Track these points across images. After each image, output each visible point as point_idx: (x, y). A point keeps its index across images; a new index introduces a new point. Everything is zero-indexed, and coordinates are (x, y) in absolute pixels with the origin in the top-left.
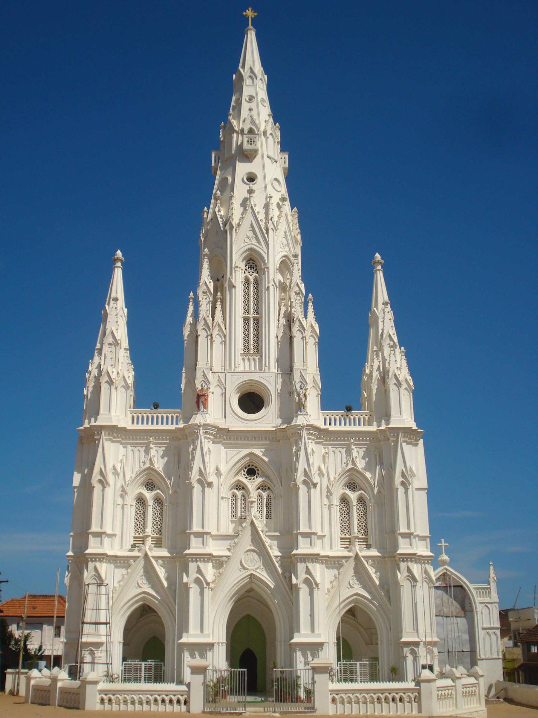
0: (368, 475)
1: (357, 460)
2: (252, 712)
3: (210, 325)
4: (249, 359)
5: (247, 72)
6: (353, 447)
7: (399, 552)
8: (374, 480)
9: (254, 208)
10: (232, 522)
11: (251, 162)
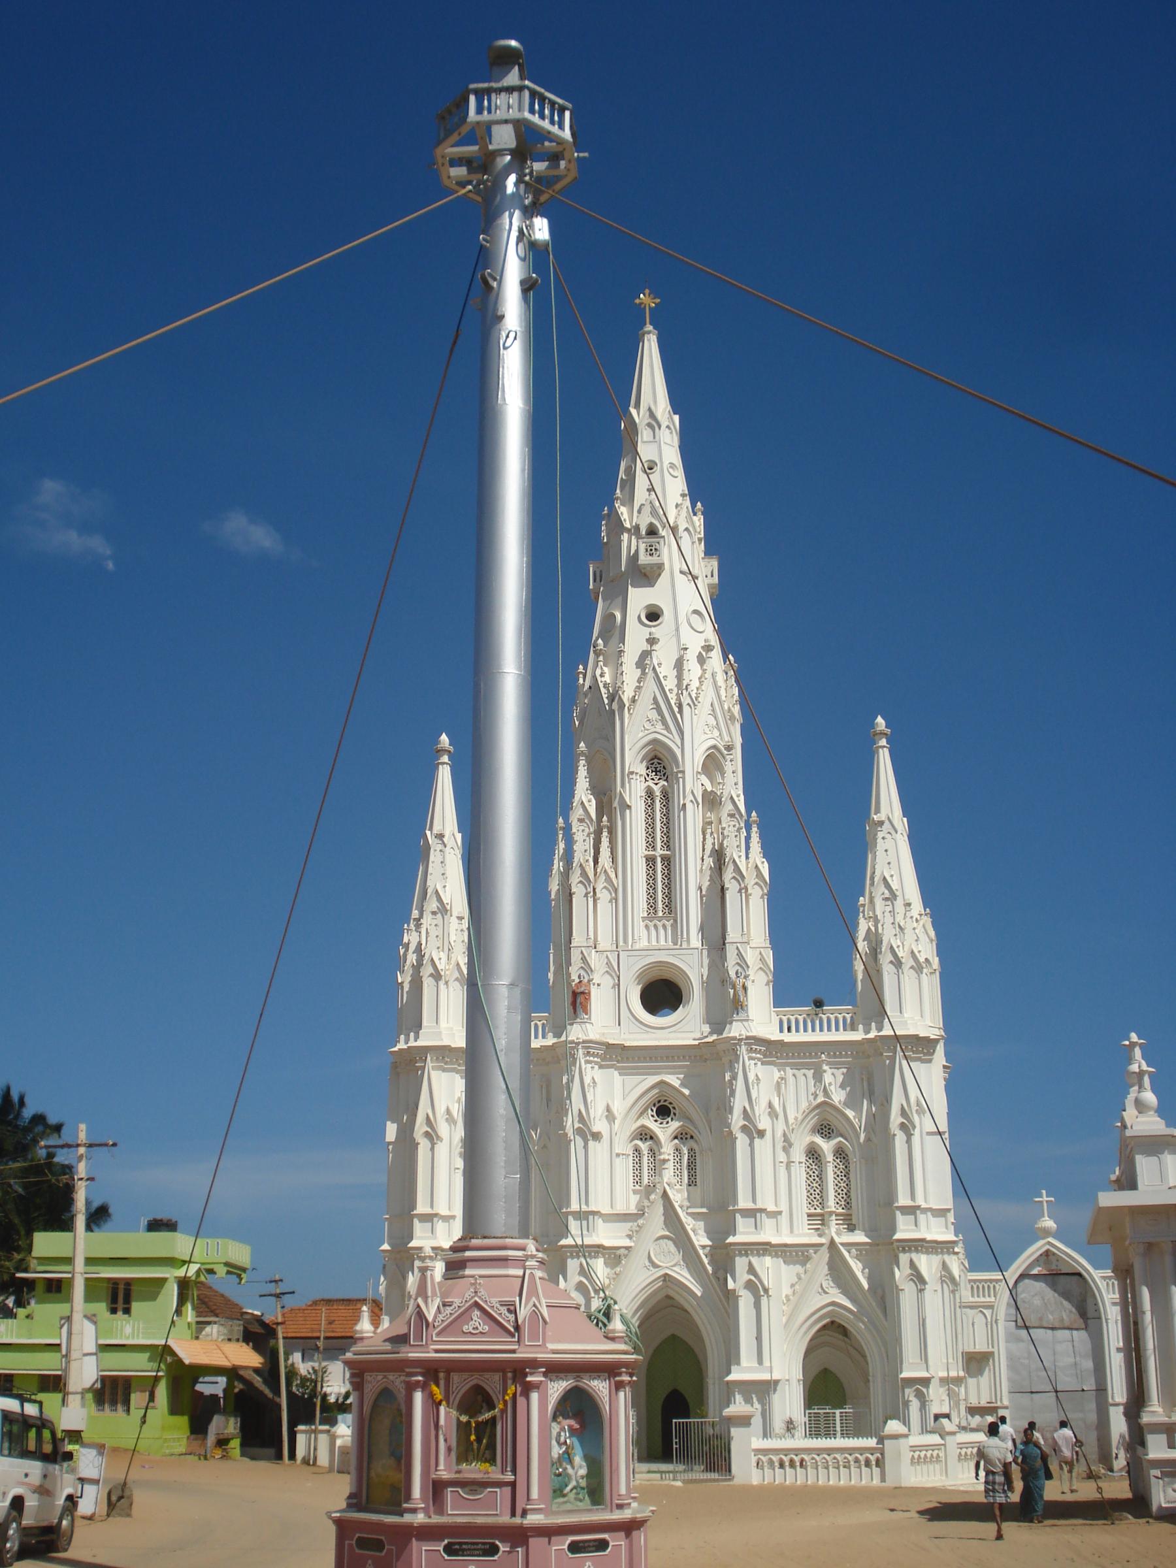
0: (850, 1114)
1: (832, 1088)
2: (644, 1480)
3: (591, 875)
4: (656, 926)
5: (644, 416)
6: (825, 1067)
7: (897, 1236)
8: (860, 1121)
9: (658, 670)
10: (635, 1192)
11: (653, 586)
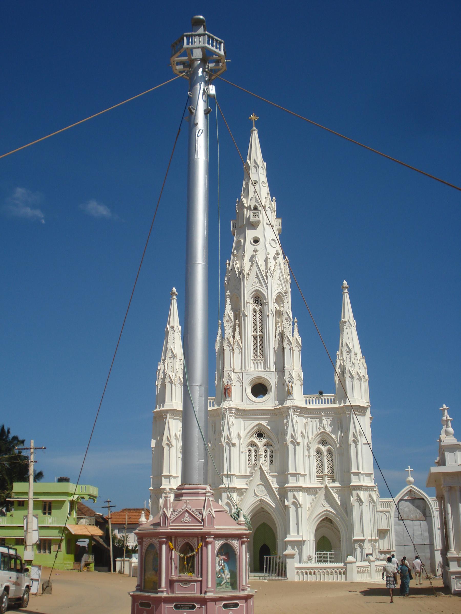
0: (333, 436)
1: (326, 426)
2: (253, 580)
3: (232, 343)
4: (257, 363)
5: (252, 163)
6: (323, 418)
7: (352, 484)
8: (337, 439)
9: (258, 262)
10: (249, 467)
11: (256, 230)
